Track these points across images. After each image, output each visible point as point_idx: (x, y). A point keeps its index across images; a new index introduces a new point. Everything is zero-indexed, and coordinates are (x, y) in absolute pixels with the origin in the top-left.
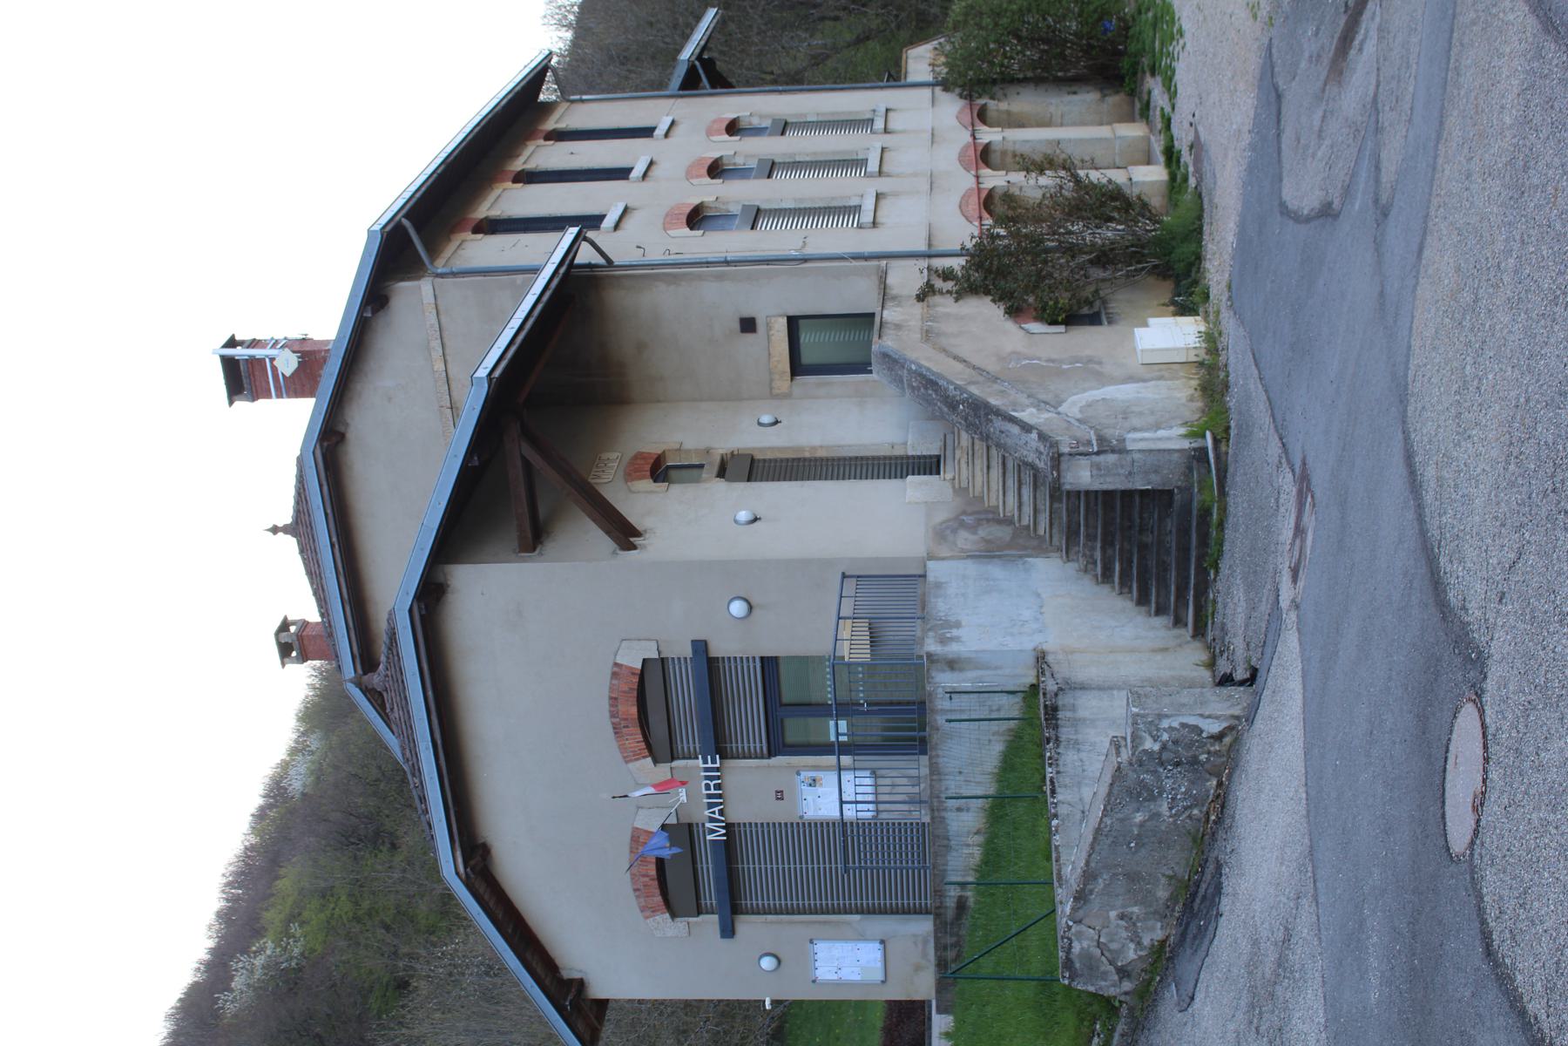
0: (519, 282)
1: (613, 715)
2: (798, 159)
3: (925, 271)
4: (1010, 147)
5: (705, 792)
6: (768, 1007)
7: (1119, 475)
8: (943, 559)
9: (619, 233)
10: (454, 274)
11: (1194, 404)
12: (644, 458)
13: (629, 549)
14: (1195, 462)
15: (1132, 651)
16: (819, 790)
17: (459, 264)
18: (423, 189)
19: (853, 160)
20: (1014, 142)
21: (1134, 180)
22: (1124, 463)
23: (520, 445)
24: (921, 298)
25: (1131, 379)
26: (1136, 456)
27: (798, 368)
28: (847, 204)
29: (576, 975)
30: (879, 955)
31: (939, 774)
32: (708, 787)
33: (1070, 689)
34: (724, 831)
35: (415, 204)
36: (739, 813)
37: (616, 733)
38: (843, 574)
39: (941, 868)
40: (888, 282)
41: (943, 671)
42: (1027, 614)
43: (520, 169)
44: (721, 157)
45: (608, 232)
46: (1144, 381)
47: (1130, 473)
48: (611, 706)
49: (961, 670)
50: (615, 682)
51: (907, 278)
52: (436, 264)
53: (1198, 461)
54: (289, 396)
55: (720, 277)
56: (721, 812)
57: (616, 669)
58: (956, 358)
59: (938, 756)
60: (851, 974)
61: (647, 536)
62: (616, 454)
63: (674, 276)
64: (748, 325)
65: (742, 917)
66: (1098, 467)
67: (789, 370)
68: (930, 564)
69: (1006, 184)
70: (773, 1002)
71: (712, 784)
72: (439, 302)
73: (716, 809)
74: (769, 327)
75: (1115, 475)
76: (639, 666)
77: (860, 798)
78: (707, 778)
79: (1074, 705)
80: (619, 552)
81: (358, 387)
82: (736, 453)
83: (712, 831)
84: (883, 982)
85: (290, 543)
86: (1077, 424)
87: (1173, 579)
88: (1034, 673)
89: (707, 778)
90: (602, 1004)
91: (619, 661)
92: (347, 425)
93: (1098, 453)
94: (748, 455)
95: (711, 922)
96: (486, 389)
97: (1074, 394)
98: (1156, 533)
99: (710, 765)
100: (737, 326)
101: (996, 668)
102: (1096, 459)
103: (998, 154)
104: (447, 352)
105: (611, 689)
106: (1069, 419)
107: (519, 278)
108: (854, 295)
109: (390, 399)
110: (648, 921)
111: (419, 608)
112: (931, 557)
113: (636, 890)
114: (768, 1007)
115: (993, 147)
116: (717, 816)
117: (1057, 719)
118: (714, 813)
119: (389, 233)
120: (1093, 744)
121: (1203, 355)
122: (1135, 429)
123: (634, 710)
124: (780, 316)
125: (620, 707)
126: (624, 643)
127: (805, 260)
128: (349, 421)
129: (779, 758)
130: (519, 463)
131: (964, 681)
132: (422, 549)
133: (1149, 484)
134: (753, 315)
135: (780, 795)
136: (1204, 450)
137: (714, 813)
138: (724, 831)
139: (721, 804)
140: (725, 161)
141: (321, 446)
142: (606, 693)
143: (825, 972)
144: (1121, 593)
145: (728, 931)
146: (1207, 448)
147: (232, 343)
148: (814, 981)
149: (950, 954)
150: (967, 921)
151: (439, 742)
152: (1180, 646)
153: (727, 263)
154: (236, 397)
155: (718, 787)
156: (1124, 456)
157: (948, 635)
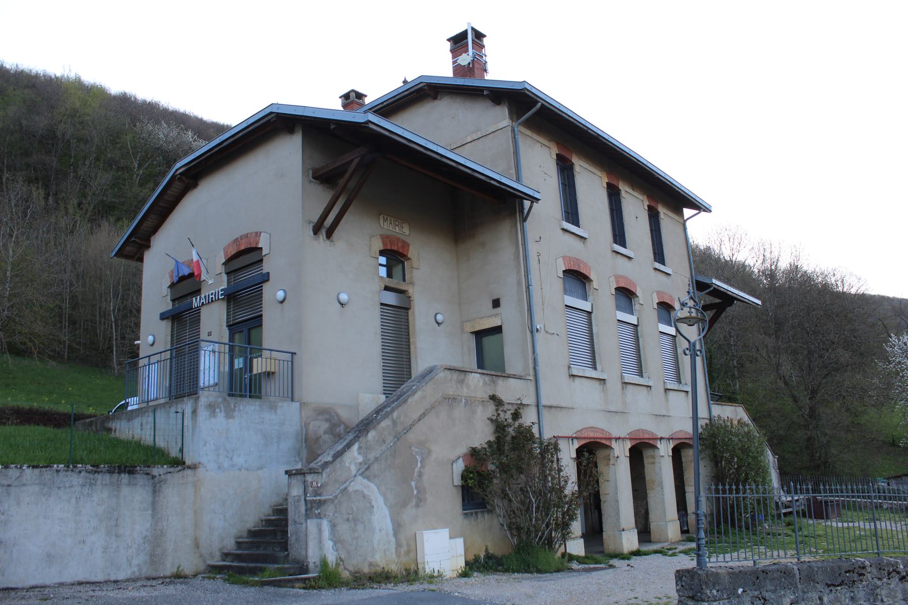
0: (511, 171)
2: (640, 339)
3: (519, 402)
4: (657, 460)
6: (136, 342)
7: (295, 515)
8: (301, 412)
10: (514, 138)
11: (367, 567)
12: (403, 247)
13: (313, 230)
15: (196, 525)
18: (571, 119)
19: (642, 370)
20: (660, 463)
21: (623, 533)
22: (301, 518)
23: (358, 157)
24: (493, 398)
25: (397, 527)
26: (304, 526)
27: (480, 335)
28: (597, 363)
33: (154, 483)
35: (581, 128)
36: (204, 312)
38: (295, 354)
40: (511, 379)
41: (192, 407)
42: (240, 460)
43: (620, 187)
45: (560, 225)
46: (396, 534)
47: (296, 522)
49: (192, 418)
52: (520, 126)
54: (453, 67)
55: (519, 284)
61: (328, 242)
62: (407, 233)
63: (518, 257)
64: (496, 303)
65: (170, 323)
66: (299, 501)
67: (475, 330)
68: (298, 404)
69: (616, 455)
71: (213, 296)
72: (499, 131)
74: (496, 315)
75: (295, 512)
76: (260, 246)
78: (215, 293)
79: (136, 485)
80: (311, 225)
81: (458, 100)
82: (411, 299)
86: (341, 488)
87: (243, 552)
88: (190, 464)
89: (215, 293)
90: (141, 260)
92: (441, 99)
93: (305, 500)
94: (410, 306)
96: (362, 121)
97: (378, 488)
98: (281, 540)
99: (220, 293)
100: (495, 297)
101: (192, 439)
103: (653, 454)
104: (476, 141)
106: (348, 483)
107: (513, 171)
108: (514, 361)
109: (453, 118)
112: (303, 405)
114: (136, 342)
115: (656, 450)
116: (202, 301)
117: (119, 473)
120: (329, 515)
121: (421, 573)
122: (333, 526)
126: (269, 235)
127: (532, 332)
129: (228, 332)
130: (352, 158)
131: (188, 421)
132: (295, 110)
133: (291, 535)
140: (636, 299)
141: (425, 86)
144: (262, 521)
146: (308, 574)
147: (479, 36)
152: (201, 556)
153: (528, 287)
156: (304, 518)
157: (218, 410)
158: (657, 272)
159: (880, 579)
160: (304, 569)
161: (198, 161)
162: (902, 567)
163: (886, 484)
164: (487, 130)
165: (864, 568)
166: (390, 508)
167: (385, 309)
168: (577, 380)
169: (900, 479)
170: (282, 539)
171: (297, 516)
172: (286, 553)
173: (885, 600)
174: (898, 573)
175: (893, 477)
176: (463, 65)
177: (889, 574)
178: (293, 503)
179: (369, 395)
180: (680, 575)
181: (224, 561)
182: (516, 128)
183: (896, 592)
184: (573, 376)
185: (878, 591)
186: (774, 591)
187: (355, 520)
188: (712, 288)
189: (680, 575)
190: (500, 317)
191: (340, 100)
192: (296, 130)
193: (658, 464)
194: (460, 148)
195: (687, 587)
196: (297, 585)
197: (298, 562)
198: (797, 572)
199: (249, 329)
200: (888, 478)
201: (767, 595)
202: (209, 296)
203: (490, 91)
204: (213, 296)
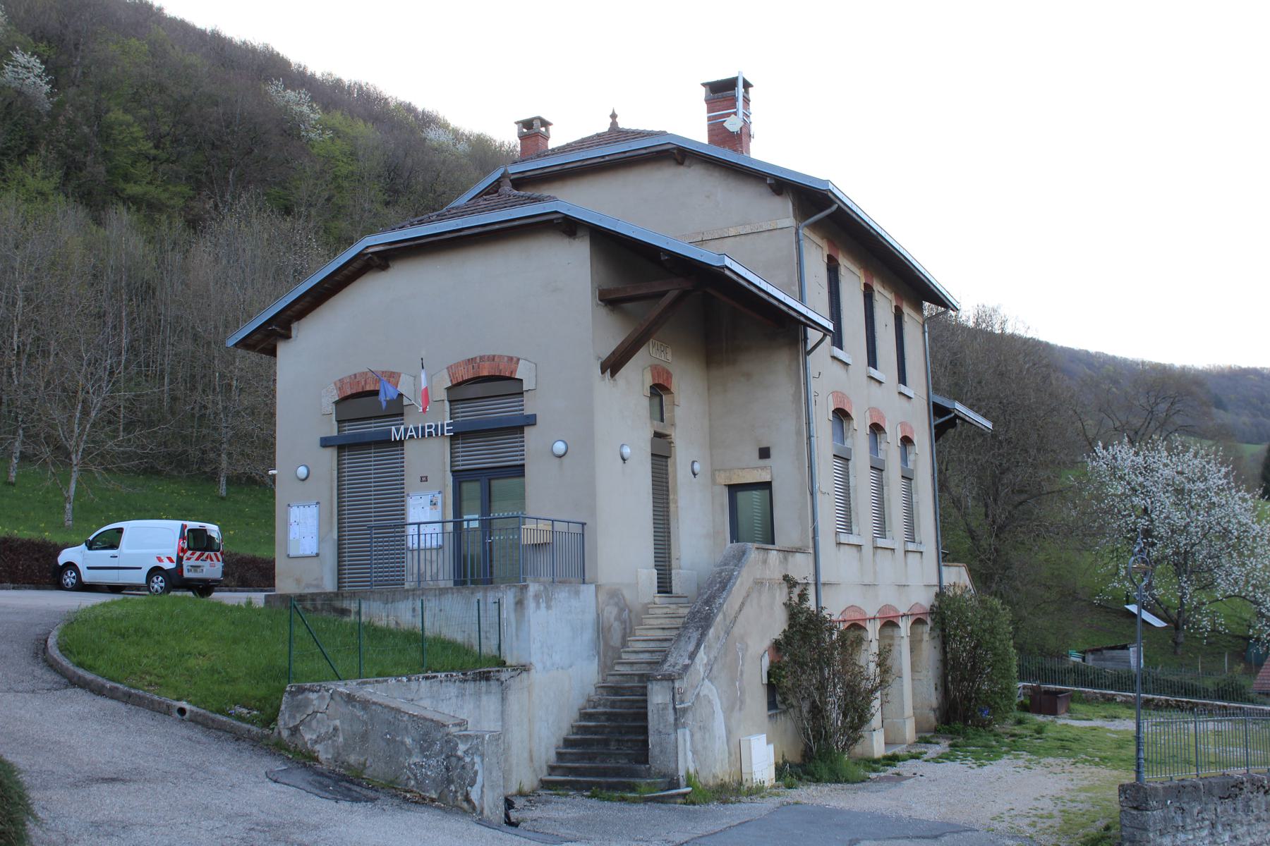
0: (793, 288)
1: (482, 358)
5: (426, 425)
6: (270, 472)
7: (659, 724)
8: (596, 596)
9: (830, 359)
10: (798, 242)
14: (669, 780)
16: (428, 508)
17: (805, 245)
18: (859, 219)
20: (900, 645)
21: (874, 733)
26: (673, 737)
29: (294, 333)
30: (308, 553)
31: (440, 595)
32: (430, 427)
33: (502, 690)
34: (398, 439)
37: (469, 360)
39: (371, 597)
41: (515, 597)
43: (840, 261)
44: (852, 419)
47: (660, 732)
48: (489, 357)
50: (506, 359)
51: (800, 568)
52: (806, 229)
53: (669, 782)
54: (709, 125)
55: (799, 433)
56: (412, 437)
57: (515, 359)
58: (743, 604)
59: (453, 594)
60: (294, 532)
64: (765, 453)
70: (274, 476)
72: (778, 231)
73: (414, 433)
74: (763, 468)
77: (422, 537)
78: (437, 426)
83: (398, 430)
84: (288, 556)
85: (604, 127)
88: (514, 663)
89: (437, 426)
90: (273, 352)
91: (521, 361)
92: (689, 167)
93: (675, 708)
94: (670, 451)
95: (332, 430)
99: (446, 428)
100: (764, 445)
102: (671, 706)
103: (891, 634)
104: (743, 237)
105: (500, 356)
107: (796, 288)
108: (788, 528)
109: (708, 197)
110: (333, 385)
111: (557, 219)
113: (355, 375)
114: (270, 472)
115: (896, 629)
116: (409, 434)
118: (411, 432)
119: (827, 195)
123: (485, 373)
124: (772, 476)
125: (488, 363)
126: (534, 365)
128: (692, 168)
130: (665, 288)
133: (653, 746)
134: (772, 457)
135: (424, 479)
136: (678, 786)
137: (411, 432)
138: (398, 439)
139: (418, 437)
140: (883, 435)
141: (674, 149)
142: (497, 353)
143: (296, 513)
144: (572, 727)
145: (326, 443)
148: (289, 505)
149: (308, 604)
150: (332, 616)
151: (462, 233)
152: (534, 770)
153: (809, 437)
154: (708, 88)
155: (430, 434)
158: (836, 362)
159: (1252, 793)
160: (674, 784)
161: (412, 243)
162: (1266, 782)
163: (1081, 660)
164: (761, 226)
165: (1242, 783)
166: (724, 712)
167: (516, 411)
168: (842, 547)
169: (1099, 653)
170: (617, 749)
171: (662, 726)
172: (648, 766)
173: (1254, 810)
174: (1264, 787)
175: (1090, 651)
176: (731, 130)
177: (1258, 788)
178: (655, 711)
179: (645, 570)
180: (1123, 789)
181: (550, 775)
182: (800, 231)
183: (1261, 803)
184: (840, 543)
185: (1250, 803)
186: (1188, 803)
187: (704, 728)
188: (953, 415)
189: (1123, 789)
190: (769, 471)
191: (516, 126)
192: (579, 234)
193: (897, 647)
194: (717, 241)
195: (1131, 799)
196: (679, 801)
197: (664, 776)
198: (1202, 787)
199: (490, 480)
200: (1084, 652)
201: (1185, 806)
202: (423, 428)
203: (775, 179)
204: (432, 430)
